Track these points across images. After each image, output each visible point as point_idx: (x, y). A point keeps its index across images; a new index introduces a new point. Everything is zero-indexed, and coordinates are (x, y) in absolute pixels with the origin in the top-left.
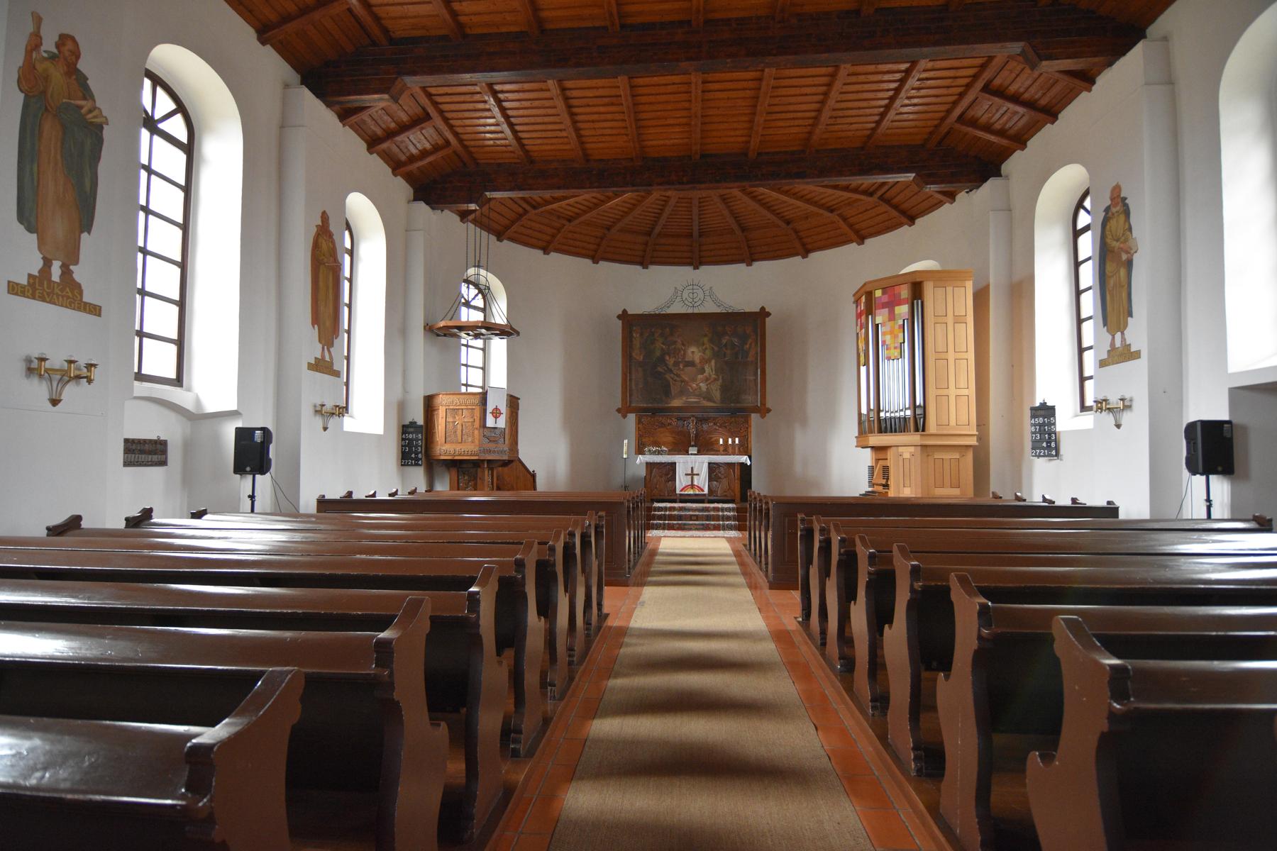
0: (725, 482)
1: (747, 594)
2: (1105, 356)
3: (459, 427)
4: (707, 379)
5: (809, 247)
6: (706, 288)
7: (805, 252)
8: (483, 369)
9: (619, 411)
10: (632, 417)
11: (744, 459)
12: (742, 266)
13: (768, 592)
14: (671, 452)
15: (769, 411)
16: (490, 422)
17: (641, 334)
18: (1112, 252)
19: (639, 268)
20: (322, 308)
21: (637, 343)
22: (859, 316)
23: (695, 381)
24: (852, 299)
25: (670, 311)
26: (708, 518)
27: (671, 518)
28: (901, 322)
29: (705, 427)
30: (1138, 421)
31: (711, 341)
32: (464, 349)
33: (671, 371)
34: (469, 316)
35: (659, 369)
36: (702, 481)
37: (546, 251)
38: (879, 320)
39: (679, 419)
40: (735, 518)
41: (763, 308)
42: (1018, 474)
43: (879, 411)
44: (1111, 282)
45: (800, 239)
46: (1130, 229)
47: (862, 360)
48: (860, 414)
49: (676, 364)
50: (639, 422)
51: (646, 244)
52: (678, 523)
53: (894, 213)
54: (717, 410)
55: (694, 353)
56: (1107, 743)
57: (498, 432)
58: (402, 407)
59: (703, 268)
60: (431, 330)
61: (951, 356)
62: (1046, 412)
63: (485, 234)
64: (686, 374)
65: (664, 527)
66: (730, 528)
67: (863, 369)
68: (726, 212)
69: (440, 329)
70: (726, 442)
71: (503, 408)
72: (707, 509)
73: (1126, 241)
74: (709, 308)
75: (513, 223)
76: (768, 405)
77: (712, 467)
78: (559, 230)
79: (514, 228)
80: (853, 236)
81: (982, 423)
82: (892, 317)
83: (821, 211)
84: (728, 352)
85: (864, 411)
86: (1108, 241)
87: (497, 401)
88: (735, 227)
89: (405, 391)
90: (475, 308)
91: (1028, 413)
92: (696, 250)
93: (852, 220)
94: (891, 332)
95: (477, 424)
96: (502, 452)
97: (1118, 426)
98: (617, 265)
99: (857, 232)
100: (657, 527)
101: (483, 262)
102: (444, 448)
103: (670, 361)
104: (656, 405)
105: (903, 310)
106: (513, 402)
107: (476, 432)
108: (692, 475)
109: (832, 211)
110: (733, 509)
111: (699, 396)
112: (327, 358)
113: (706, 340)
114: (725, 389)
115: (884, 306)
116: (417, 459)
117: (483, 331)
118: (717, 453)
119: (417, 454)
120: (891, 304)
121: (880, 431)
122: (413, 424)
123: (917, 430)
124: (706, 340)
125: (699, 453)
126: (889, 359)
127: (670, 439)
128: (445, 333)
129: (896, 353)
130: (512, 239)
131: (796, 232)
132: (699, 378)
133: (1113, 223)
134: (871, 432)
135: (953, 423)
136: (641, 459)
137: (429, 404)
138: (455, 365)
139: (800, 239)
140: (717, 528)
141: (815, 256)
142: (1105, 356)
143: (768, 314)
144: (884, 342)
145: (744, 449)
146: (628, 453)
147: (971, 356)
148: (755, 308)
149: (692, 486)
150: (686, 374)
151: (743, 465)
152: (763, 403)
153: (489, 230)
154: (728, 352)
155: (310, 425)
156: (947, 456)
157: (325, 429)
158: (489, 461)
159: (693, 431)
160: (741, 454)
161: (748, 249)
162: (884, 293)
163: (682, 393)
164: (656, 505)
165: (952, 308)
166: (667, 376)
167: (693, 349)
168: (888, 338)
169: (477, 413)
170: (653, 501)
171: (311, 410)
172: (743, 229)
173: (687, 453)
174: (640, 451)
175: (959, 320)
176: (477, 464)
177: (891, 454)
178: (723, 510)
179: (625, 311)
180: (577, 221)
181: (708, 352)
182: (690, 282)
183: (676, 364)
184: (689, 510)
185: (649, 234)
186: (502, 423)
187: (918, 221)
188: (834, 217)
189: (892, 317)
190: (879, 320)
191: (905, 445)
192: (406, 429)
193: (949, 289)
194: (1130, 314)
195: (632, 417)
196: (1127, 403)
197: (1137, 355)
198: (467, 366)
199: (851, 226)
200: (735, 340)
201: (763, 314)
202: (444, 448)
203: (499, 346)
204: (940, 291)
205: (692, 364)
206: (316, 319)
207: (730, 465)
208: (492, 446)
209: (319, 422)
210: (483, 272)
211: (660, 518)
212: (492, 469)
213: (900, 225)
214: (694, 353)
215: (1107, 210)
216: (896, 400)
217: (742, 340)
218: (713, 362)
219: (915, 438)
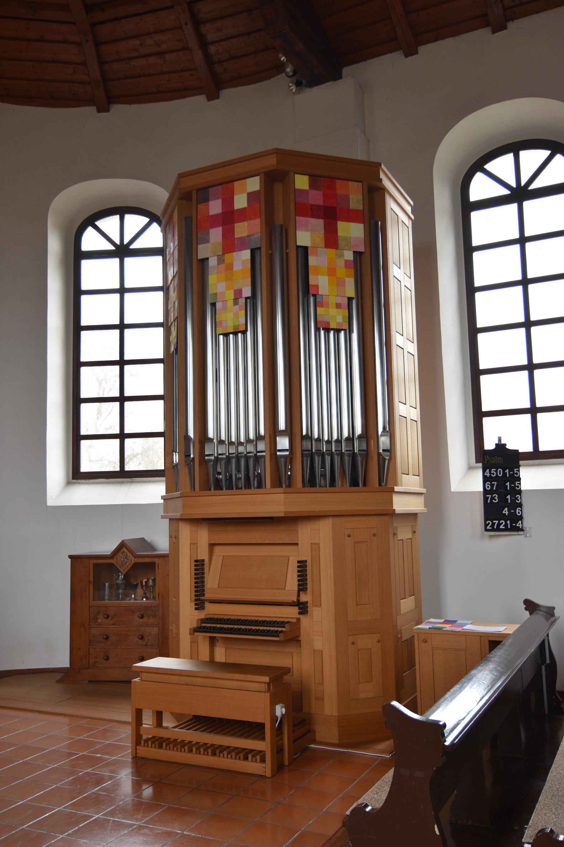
82: (331, 240)
94: (331, 272)
115: (313, 212)
162: (313, 185)
189: (331, 240)
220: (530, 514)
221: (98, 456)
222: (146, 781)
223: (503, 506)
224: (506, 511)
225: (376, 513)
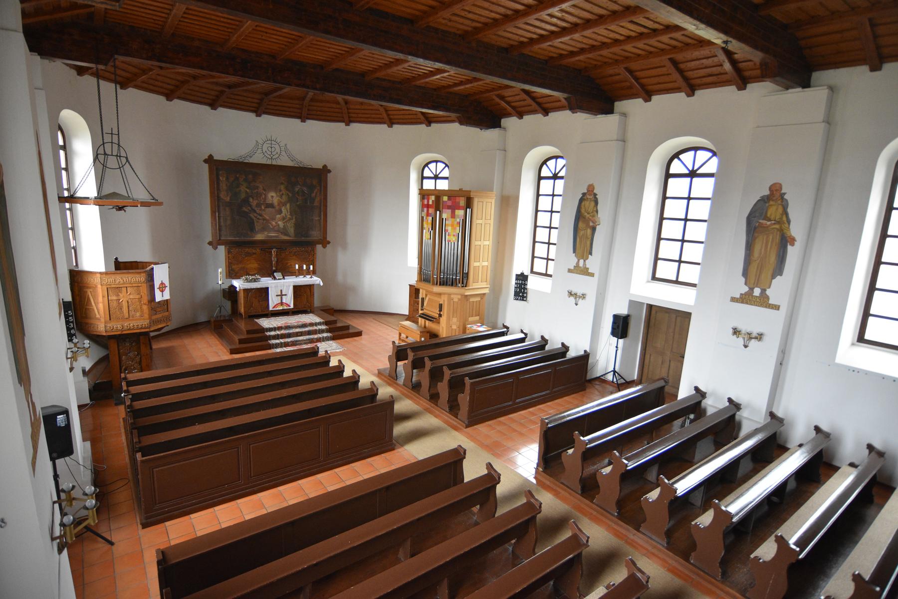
3: (125, 305)
4: (284, 218)
6: (282, 144)
10: (222, 249)
15: (329, 243)
16: (159, 297)
17: (227, 179)
18: (584, 218)
19: (208, 108)
21: (223, 186)
23: (279, 217)
25: (252, 160)
30: (588, 306)
31: (287, 188)
33: (255, 211)
35: (244, 209)
36: (289, 300)
40: (328, 331)
41: (325, 166)
46: (597, 212)
50: (229, 252)
55: (273, 197)
56: (449, 381)
64: (267, 213)
73: (593, 216)
74: (284, 161)
82: (453, 216)
91: (514, 278)
94: (452, 226)
95: (145, 299)
97: (576, 304)
99: (390, 119)
102: (101, 324)
103: (254, 203)
107: (145, 307)
108: (282, 295)
111: (278, 231)
113: (282, 187)
114: (297, 226)
115: (449, 207)
120: (453, 208)
124: (282, 187)
132: (277, 220)
133: (586, 204)
141: (355, 126)
143: (329, 171)
148: (582, 353)
149: (282, 303)
150: (267, 213)
152: (325, 237)
154: (300, 198)
162: (449, 199)
163: (264, 229)
166: (251, 215)
167: (273, 194)
169: (144, 290)
179: (211, 157)
182: (269, 137)
183: (259, 205)
189: (453, 216)
190: (444, 216)
194: (591, 254)
195: (222, 249)
197: (592, 275)
200: (305, 189)
205: (271, 206)
213: (421, 123)
215: (584, 194)
217: (310, 187)
218: (288, 206)
220: (530, 296)
221: (666, 270)
222: (647, 481)
223: (521, 293)
225: (376, 317)
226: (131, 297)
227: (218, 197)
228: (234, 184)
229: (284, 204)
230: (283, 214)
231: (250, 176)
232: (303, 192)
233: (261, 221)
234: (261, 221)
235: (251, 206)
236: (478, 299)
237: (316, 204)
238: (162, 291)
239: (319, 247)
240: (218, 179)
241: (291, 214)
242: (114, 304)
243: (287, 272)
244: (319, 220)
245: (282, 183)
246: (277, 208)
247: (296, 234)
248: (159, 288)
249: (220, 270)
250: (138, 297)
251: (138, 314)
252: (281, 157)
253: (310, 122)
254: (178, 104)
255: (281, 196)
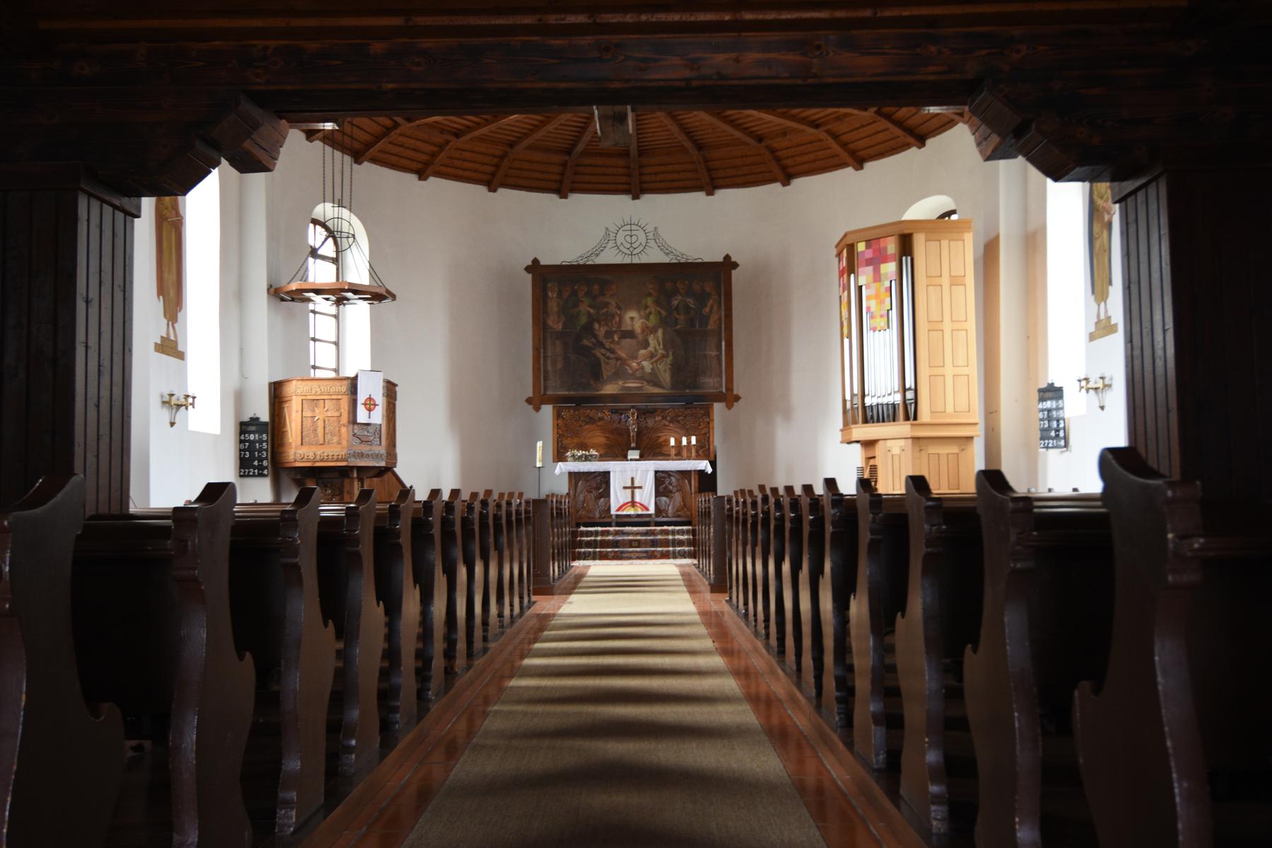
0: (678, 497)
1: (687, 596)
2: (1093, 329)
3: (320, 424)
4: (652, 356)
5: (791, 170)
6: (650, 228)
7: (786, 178)
8: (337, 344)
9: (529, 401)
10: (548, 410)
11: (705, 465)
12: (700, 196)
13: (708, 596)
14: (602, 458)
15: (737, 398)
16: (362, 416)
17: (560, 294)
19: (554, 197)
20: (166, 275)
21: (553, 306)
22: (841, 274)
23: (634, 353)
24: (835, 252)
26: (654, 543)
27: (604, 544)
28: (888, 284)
29: (650, 423)
31: (657, 303)
32: (311, 315)
33: (602, 345)
34: (321, 273)
35: (585, 342)
36: (647, 497)
37: (422, 175)
38: (862, 280)
39: (615, 411)
40: (690, 543)
41: (727, 257)
42: (1033, 469)
43: (863, 396)
44: (1097, 244)
45: (778, 160)
47: (844, 334)
48: (844, 401)
49: (609, 335)
50: (558, 415)
51: (564, 165)
52: (615, 550)
53: (898, 132)
54: (667, 398)
55: (633, 319)
57: (371, 429)
58: (240, 398)
59: (647, 198)
60: (277, 294)
61: (947, 326)
62: (1052, 392)
63: (338, 154)
65: (594, 557)
66: (683, 555)
67: (846, 341)
68: (674, 129)
69: (288, 293)
70: (679, 442)
71: (380, 399)
72: (653, 533)
75: (378, 138)
76: (737, 390)
77: (660, 477)
78: (441, 147)
79: (379, 146)
80: (844, 155)
81: (991, 412)
82: (877, 277)
83: (802, 127)
84: (681, 318)
85: (848, 397)
86: (1095, 197)
87: (371, 388)
88: (688, 145)
89: (243, 376)
90: (324, 258)
92: (635, 175)
93: (845, 138)
94: (877, 296)
95: (345, 419)
96: (377, 456)
98: (523, 193)
99: (853, 153)
100: (585, 557)
101: (346, 202)
102: (299, 452)
103: (601, 330)
104: (581, 393)
105: (889, 268)
106: (390, 390)
107: (344, 430)
108: (633, 488)
109: (817, 127)
110: (688, 532)
111: (642, 378)
112: (172, 338)
114: (676, 369)
115: (869, 262)
116: (261, 468)
117: (350, 295)
118: (666, 457)
119: (261, 460)
120: (877, 260)
121: (866, 421)
122: (254, 420)
123: (907, 418)
124: (650, 301)
125: (642, 457)
126: (874, 330)
127: (601, 440)
128: (289, 297)
129: (883, 322)
130: (374, 160)
131: (773, 151)
134: (855, 422)
135: (950, 409)
136: (562, 468)
137: (277, 393)
138: (302, 340)
139: (778, 160)
140: (665, 556)
141: (801, 184)
142: (1093, 329)
143: (735, 265)
144: (868, 309)
145: (704, 450)
146: (543, 460)
147: (972, 325)
149: (633, 503)
151: (701, 473)
152: (730, 389)
153: (344, 149)
155: (159, 416)
156: (944, 450)
157: (172, 424)
158: (360, 469)
159: (633, 428)
160: (698, 457)
161: (708, 175)
162: (868, 247)
163: (618, 374)
164: (582, 529)
165: (949, 267)
166: (598, 352)
168: (873, 303)
170: (578, 525)
171: (159, 401)
172: (700, 147)
173: (625, 458)
174: (560, 456)
175: (956, 281)
176: (344, 472)
177: (879, 450)
178: (673, 533)
179: (535, 261)
180: (468, 137)
181: (653, 320)
182: (627, 220)
183: (609, 335)
184: (628, 534)
185: (568, 152)
186: (378, 417)
187: (929, 142)
188: (820, 133)
189: (877, 277)
190: (862, 280)
191: (894, 434)
192: (244, 427)
193: (945, 243)
195: (548, 410)
196: (1107, 382)
198: (314, 340)
199: (844, 145)
200: (690, 301)
201: (728, 264)
202: (299, 452)
203: (358, 311)
204: (933, 245)
205: (630, 334)
206: (161, 291)
207: (685, 474)
208: (365, 449)
209: (165, 415)
210: (345, 213)
211: (589, 544)
212: (361, 480)
213: (905, 146)
214: (633, 319)
216: (883, 387)
217: (699, 298)
218: (660, 333)
219: (902, 428)
224: (256, 463)
226: (329, 414)
227: (545, 324)
228: (568, 302)
229: (653, 330)
230: (651, 349)
231: (596, 287)
232: (687, 308)
233: (613, 362)
234: (613, 362)
235: (595, 336)
236: (954, 449)
237: (711, 326)
238: (370, 410)
239: (718, 408)
240: (546, 296)
241: (665, 348)
242: (308, 423)
243: (651, 450)
244: (719, 357)
245: (650, 295)
246: (641, 337)
247: (674, 386)
248: (365, 404)
249: (539, 444)
250: (337, 414)
251: (335, 439)
252: (648, 250)
253: (721, 194)
254: (507, 196)
255: (647, 318)
